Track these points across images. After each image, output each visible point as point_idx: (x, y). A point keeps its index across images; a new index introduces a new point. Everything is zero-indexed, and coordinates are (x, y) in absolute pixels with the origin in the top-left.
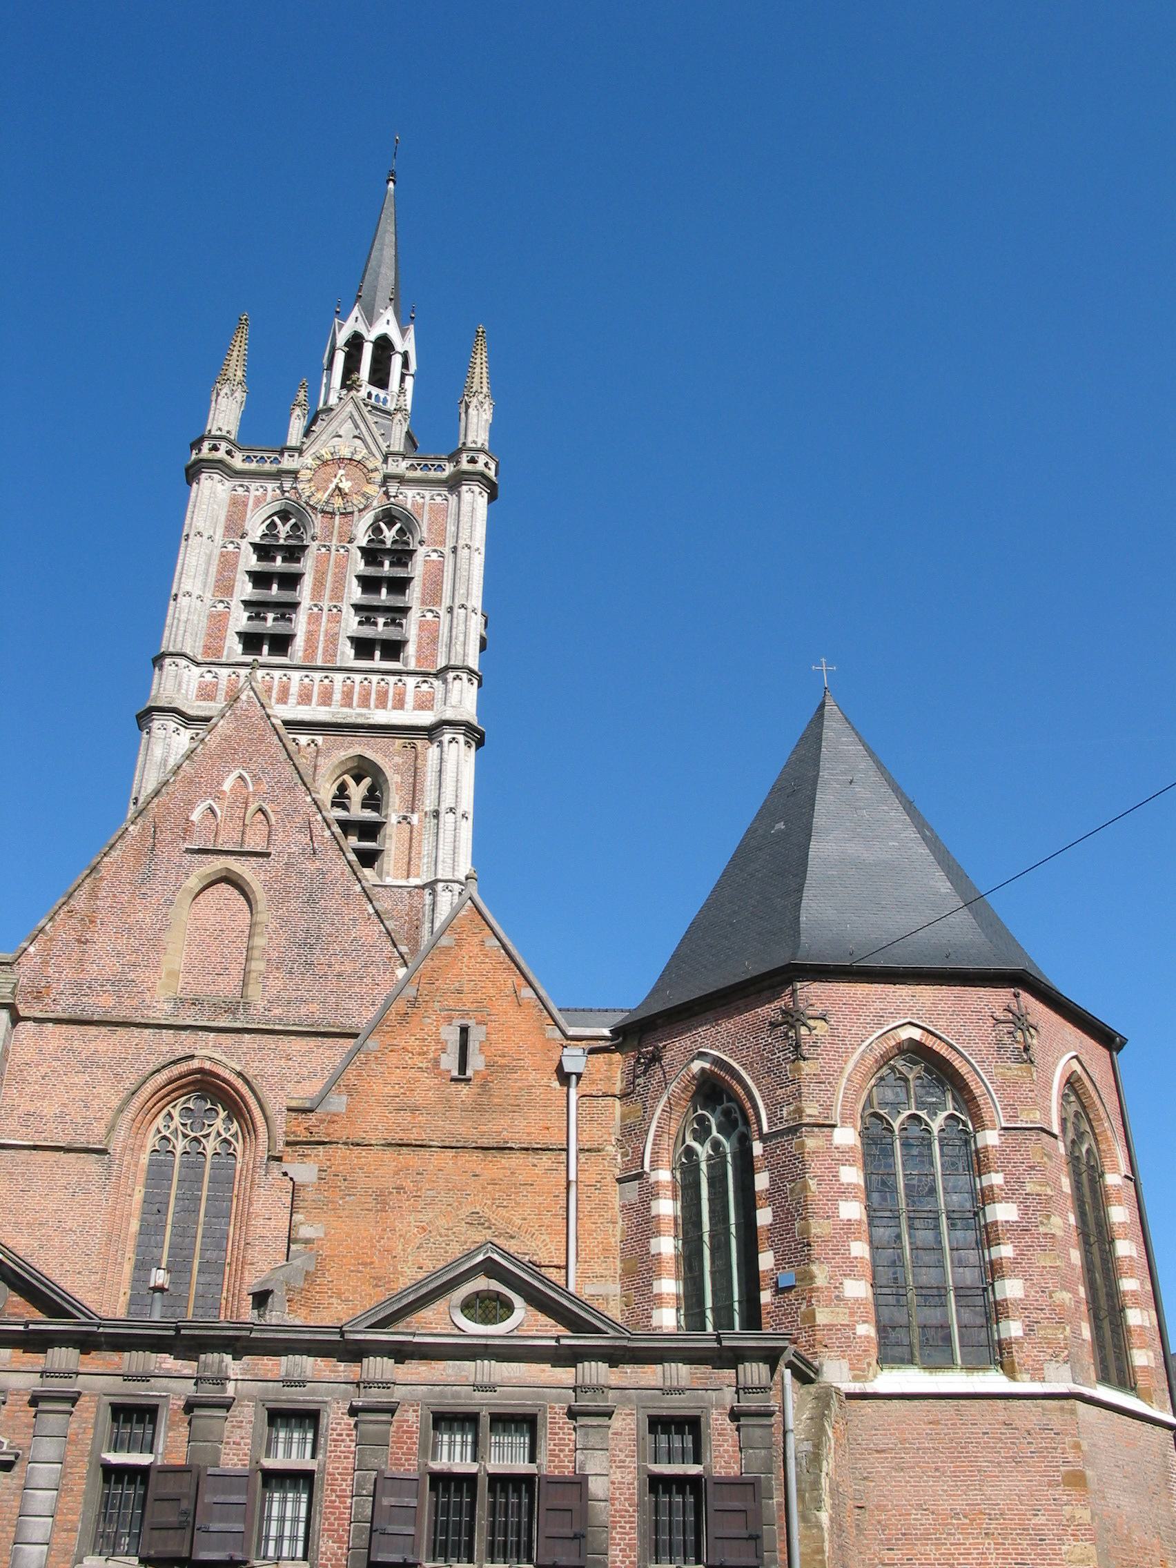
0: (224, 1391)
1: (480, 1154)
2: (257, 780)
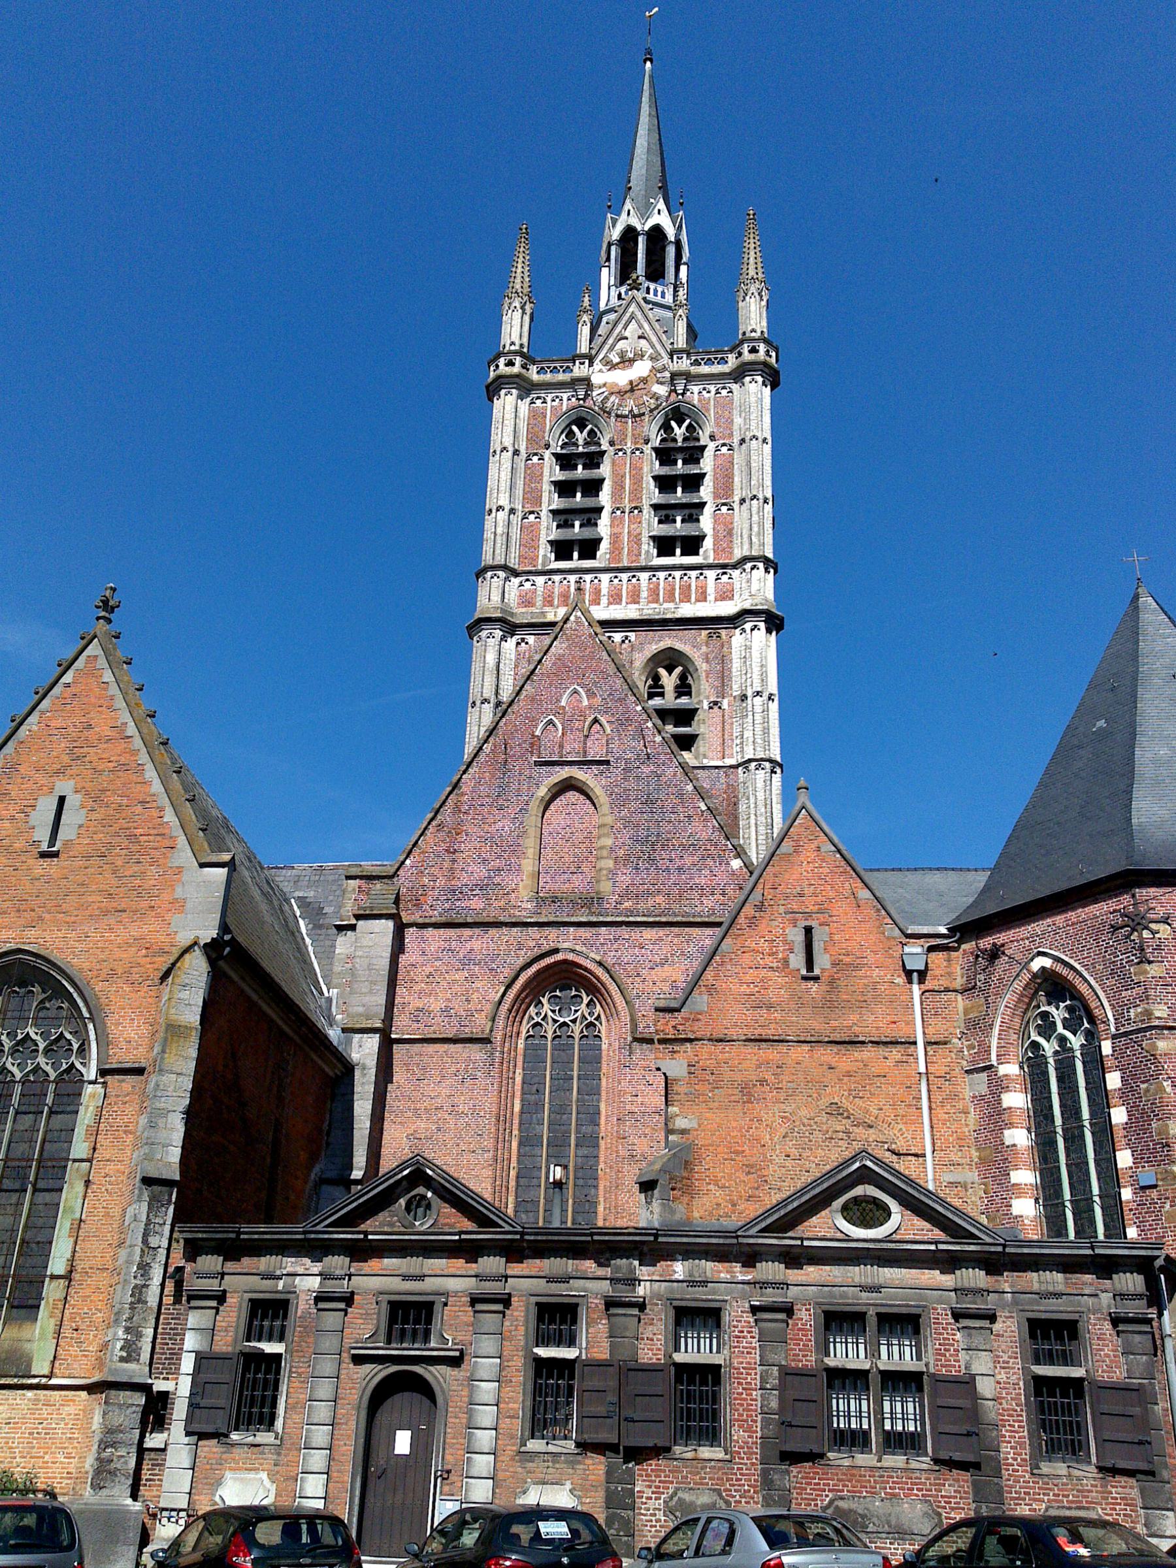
0: (634, 1291)
1: (835, 1048)
2: (591, 694)
